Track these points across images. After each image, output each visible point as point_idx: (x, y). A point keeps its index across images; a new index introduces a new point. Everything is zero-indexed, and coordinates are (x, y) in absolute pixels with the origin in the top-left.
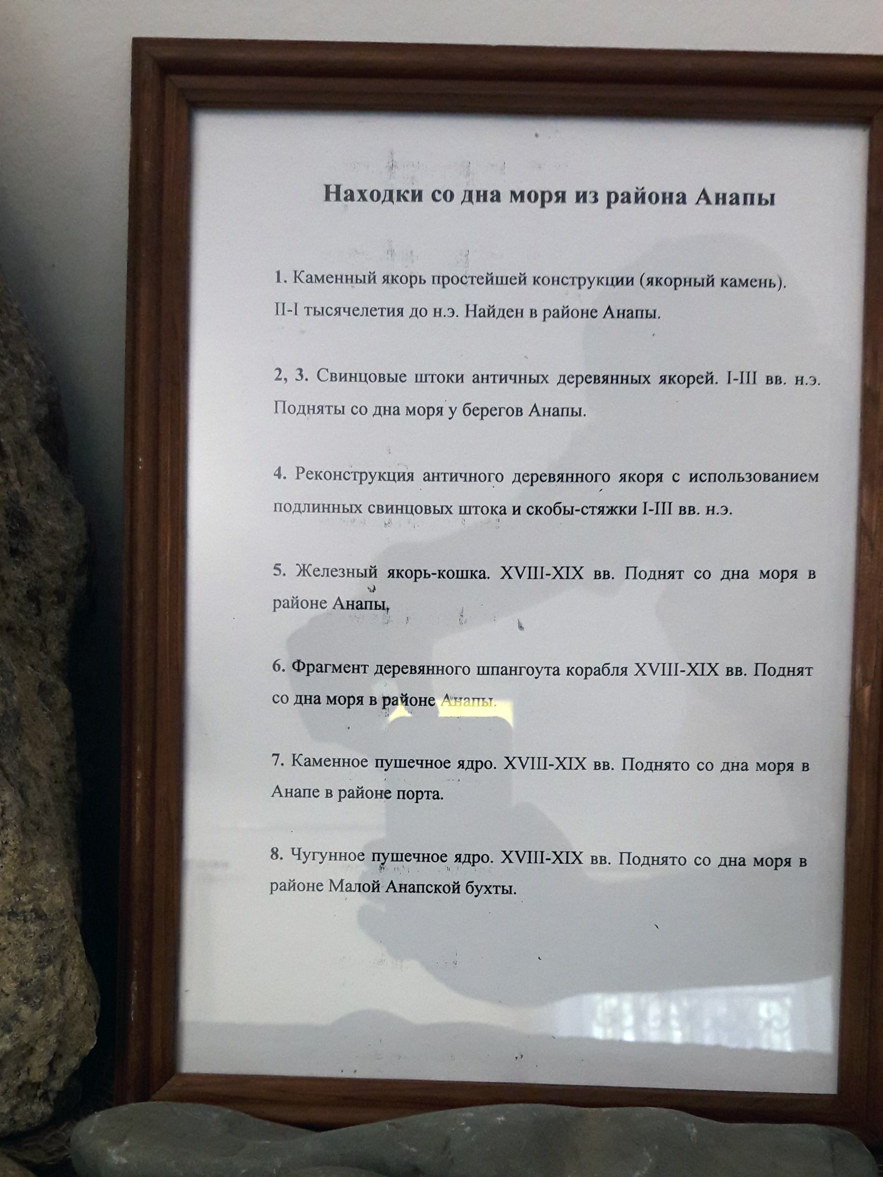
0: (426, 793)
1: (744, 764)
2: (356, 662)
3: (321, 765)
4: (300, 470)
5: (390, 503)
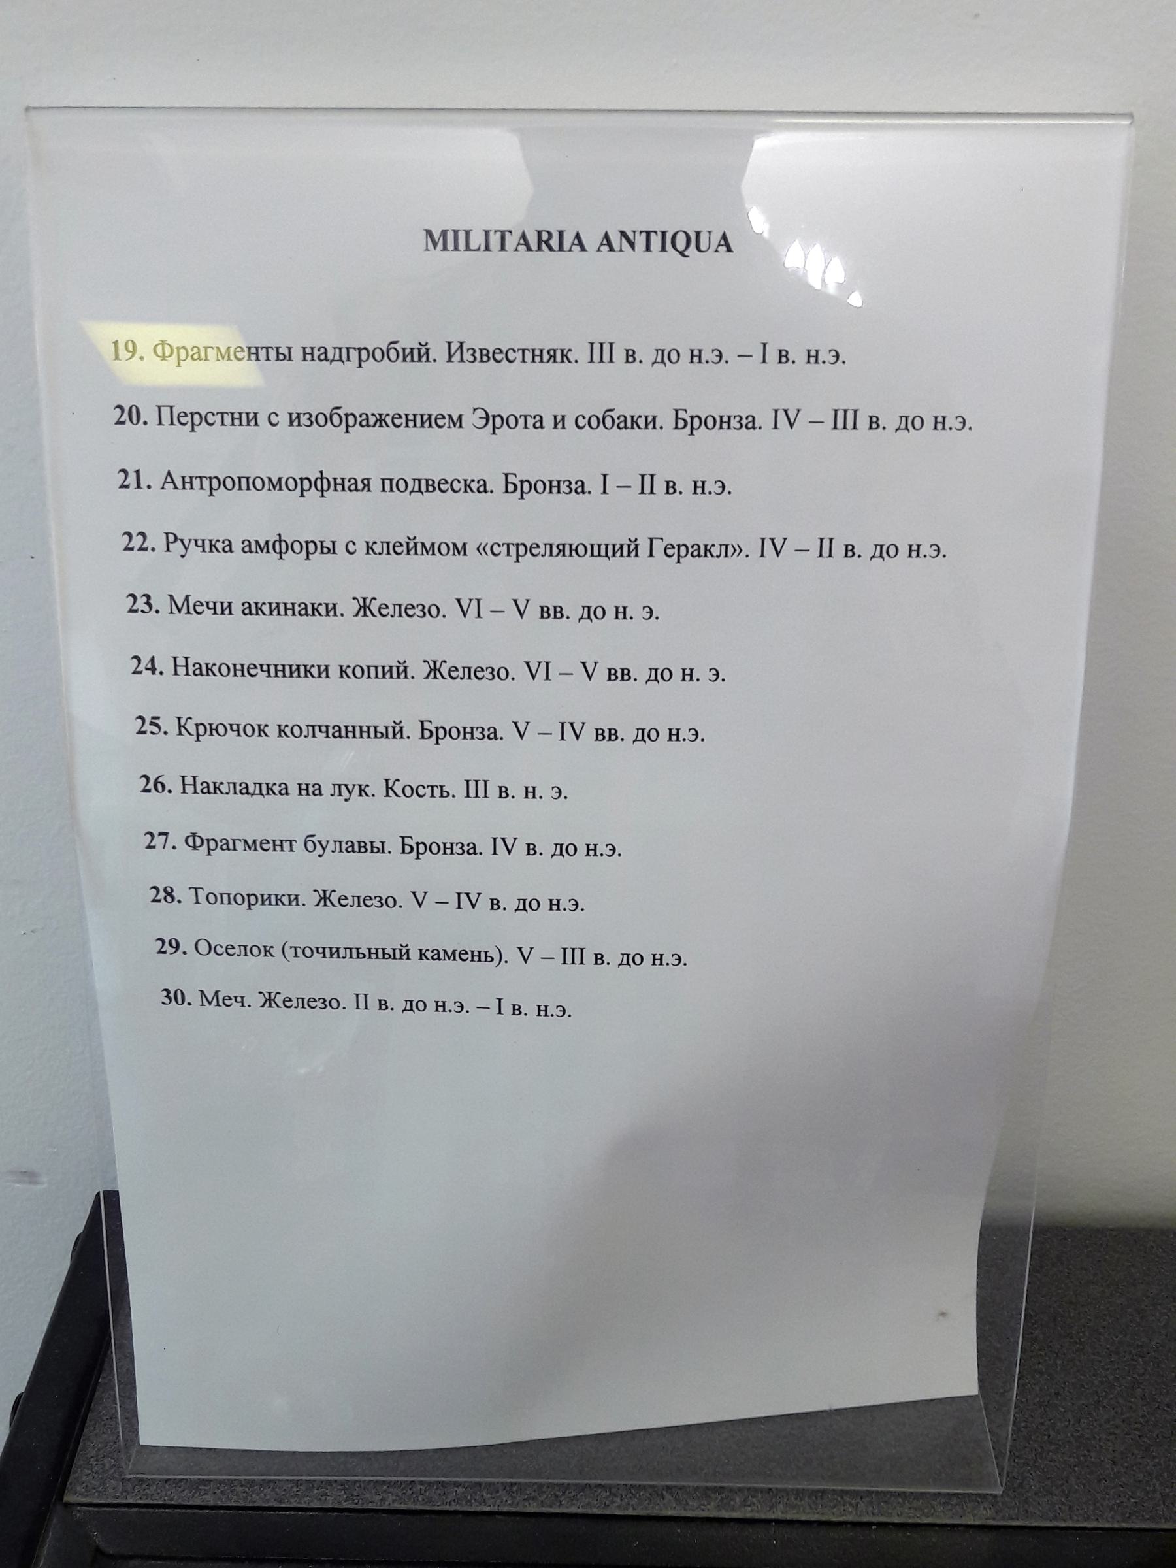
0: (523, 418)
2: (278, 837)
3: (229, 359)
4: (171, 539)
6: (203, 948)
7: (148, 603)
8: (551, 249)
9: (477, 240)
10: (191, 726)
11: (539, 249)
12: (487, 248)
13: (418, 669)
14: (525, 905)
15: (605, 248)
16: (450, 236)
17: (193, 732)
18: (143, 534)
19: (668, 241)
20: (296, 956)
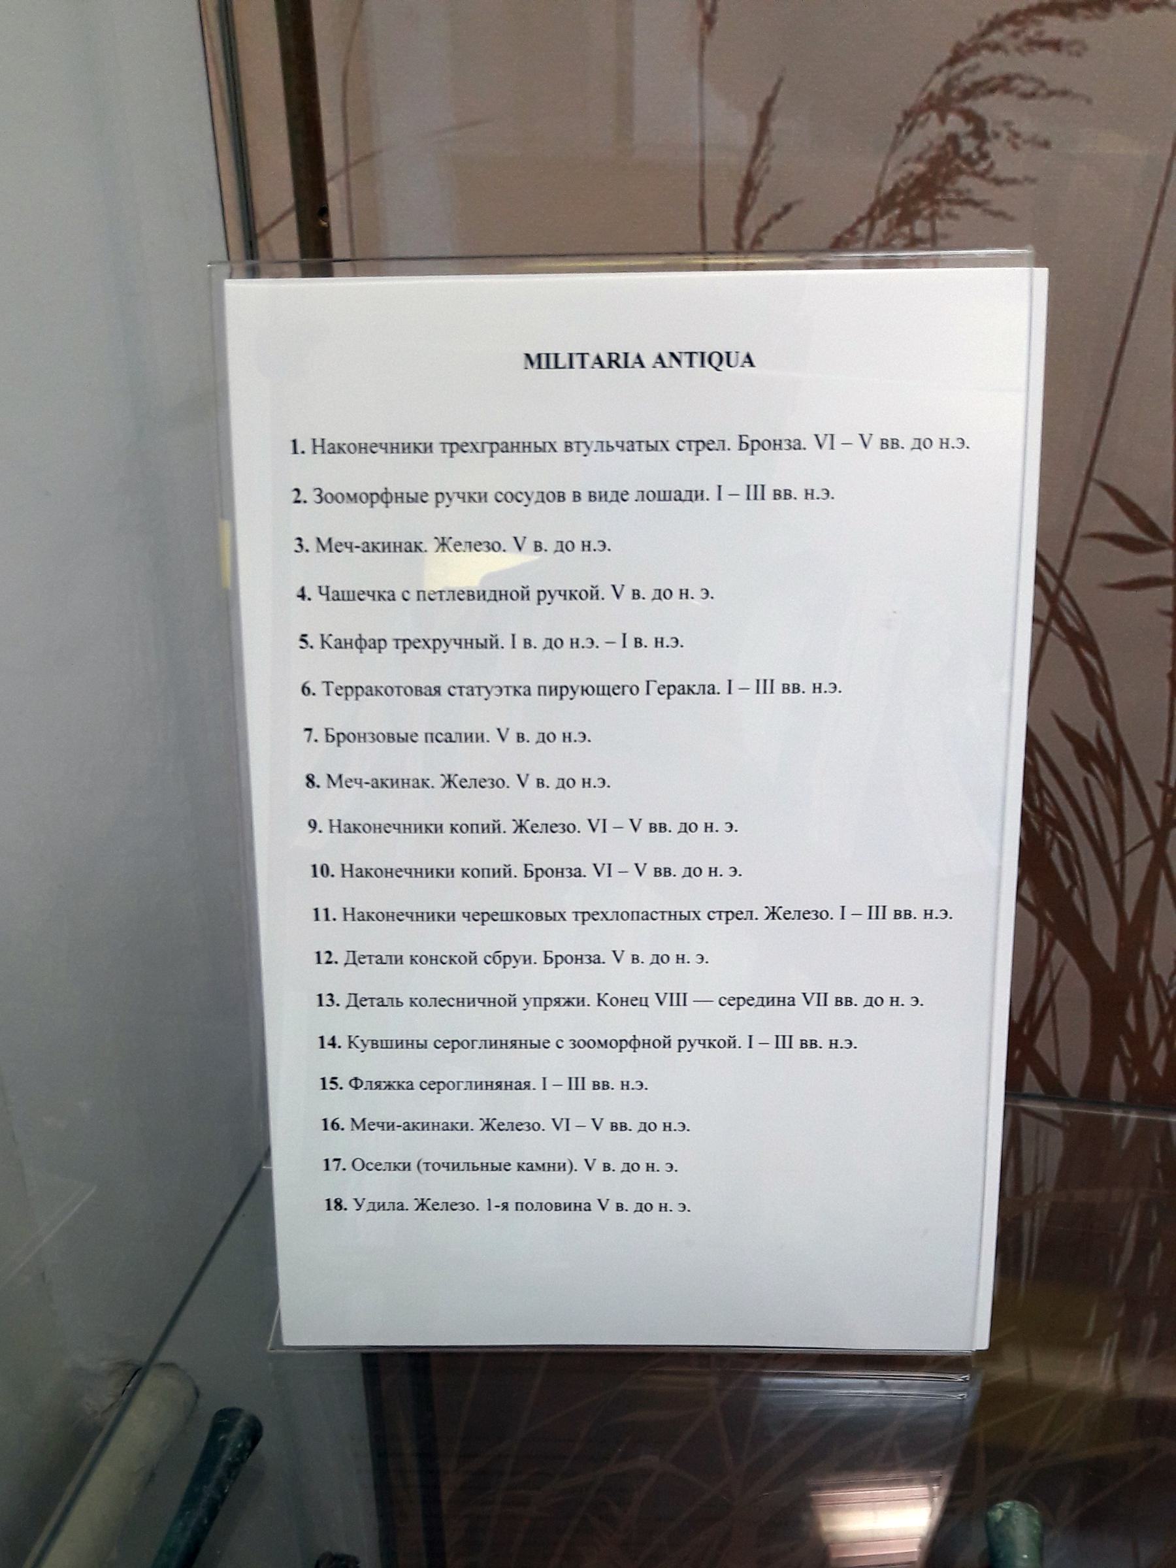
1: (791, 999)
5: (431, 923)
6: (358, 1164)
7: (332, 1000)
8: (618, 366)
9: (563, 360)
11: (610, 366)
12: (571, 367)
13: (508, 826)
14: (630, 1168)
15: (659, 366)
16: (544, 358)
18: (329, 952)
19: (706, 359)
20: (427, 1170)
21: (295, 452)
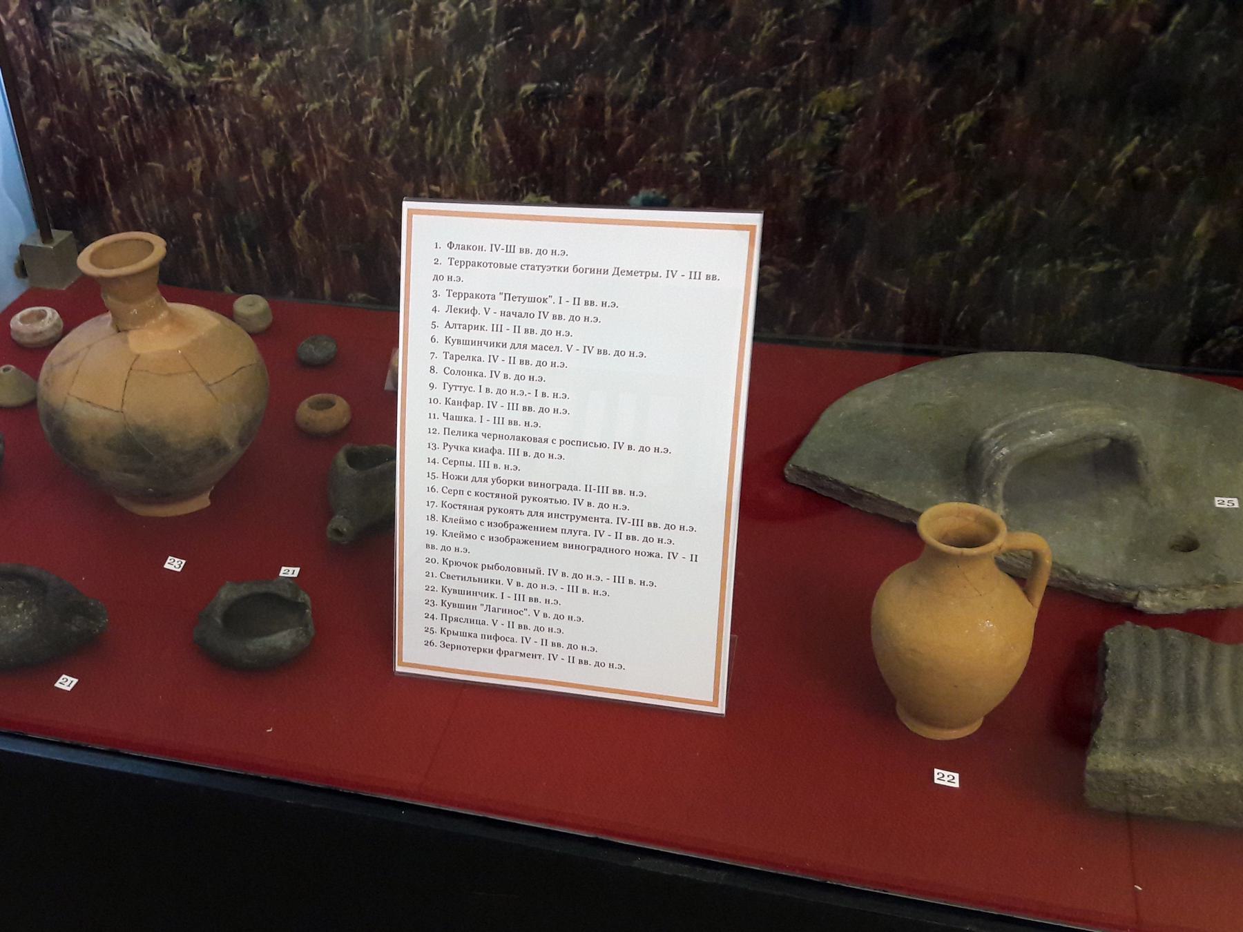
10: (448, 561)
17: (448, 563)
21: (436, 247)
